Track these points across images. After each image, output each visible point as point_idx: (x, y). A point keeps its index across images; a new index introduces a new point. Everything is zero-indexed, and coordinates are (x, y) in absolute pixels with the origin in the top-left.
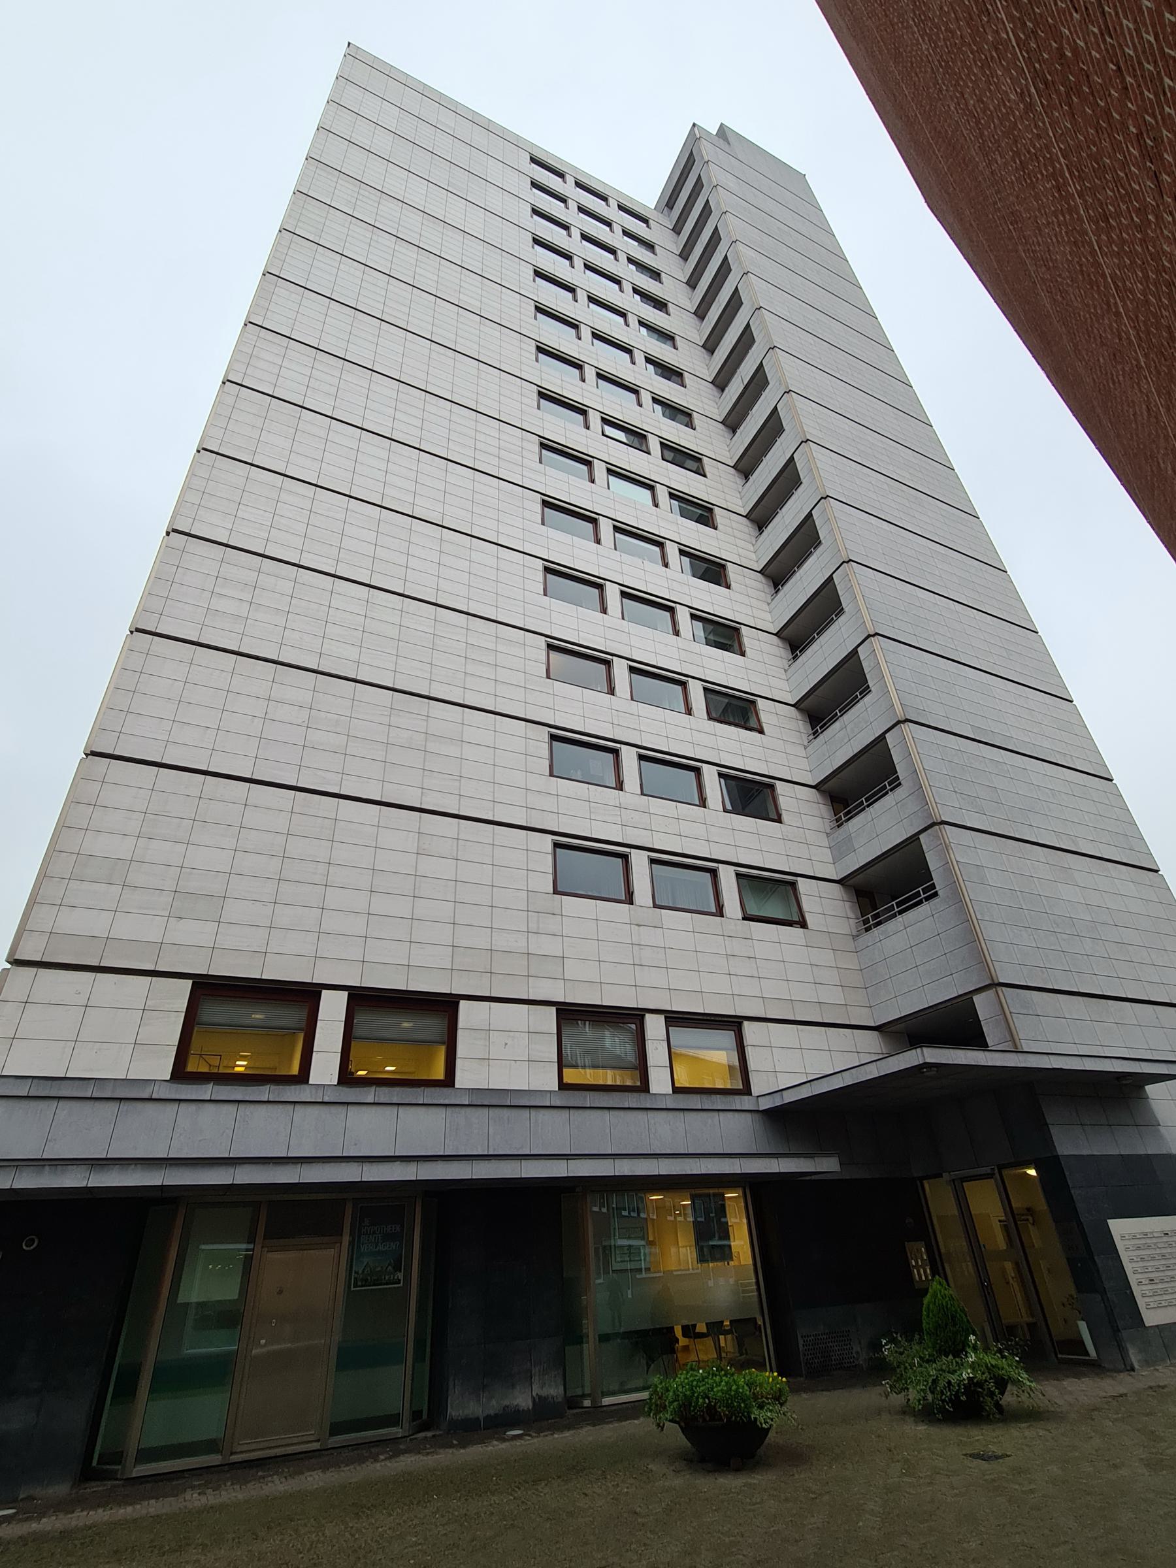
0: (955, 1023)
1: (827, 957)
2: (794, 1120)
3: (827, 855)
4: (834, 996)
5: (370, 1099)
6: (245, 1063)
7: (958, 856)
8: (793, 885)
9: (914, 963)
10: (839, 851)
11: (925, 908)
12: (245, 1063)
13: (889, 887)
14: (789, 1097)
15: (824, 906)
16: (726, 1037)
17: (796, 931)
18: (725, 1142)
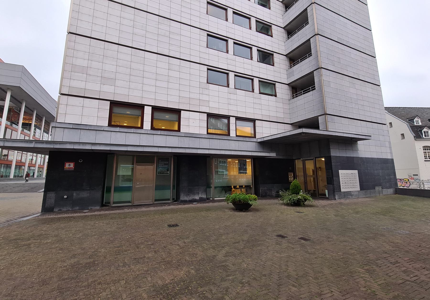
0: (313, 123)
1: (281, 105)
9: (305, 107)
10: (289, 76)
16: (251, 124)
17: (273, 98)
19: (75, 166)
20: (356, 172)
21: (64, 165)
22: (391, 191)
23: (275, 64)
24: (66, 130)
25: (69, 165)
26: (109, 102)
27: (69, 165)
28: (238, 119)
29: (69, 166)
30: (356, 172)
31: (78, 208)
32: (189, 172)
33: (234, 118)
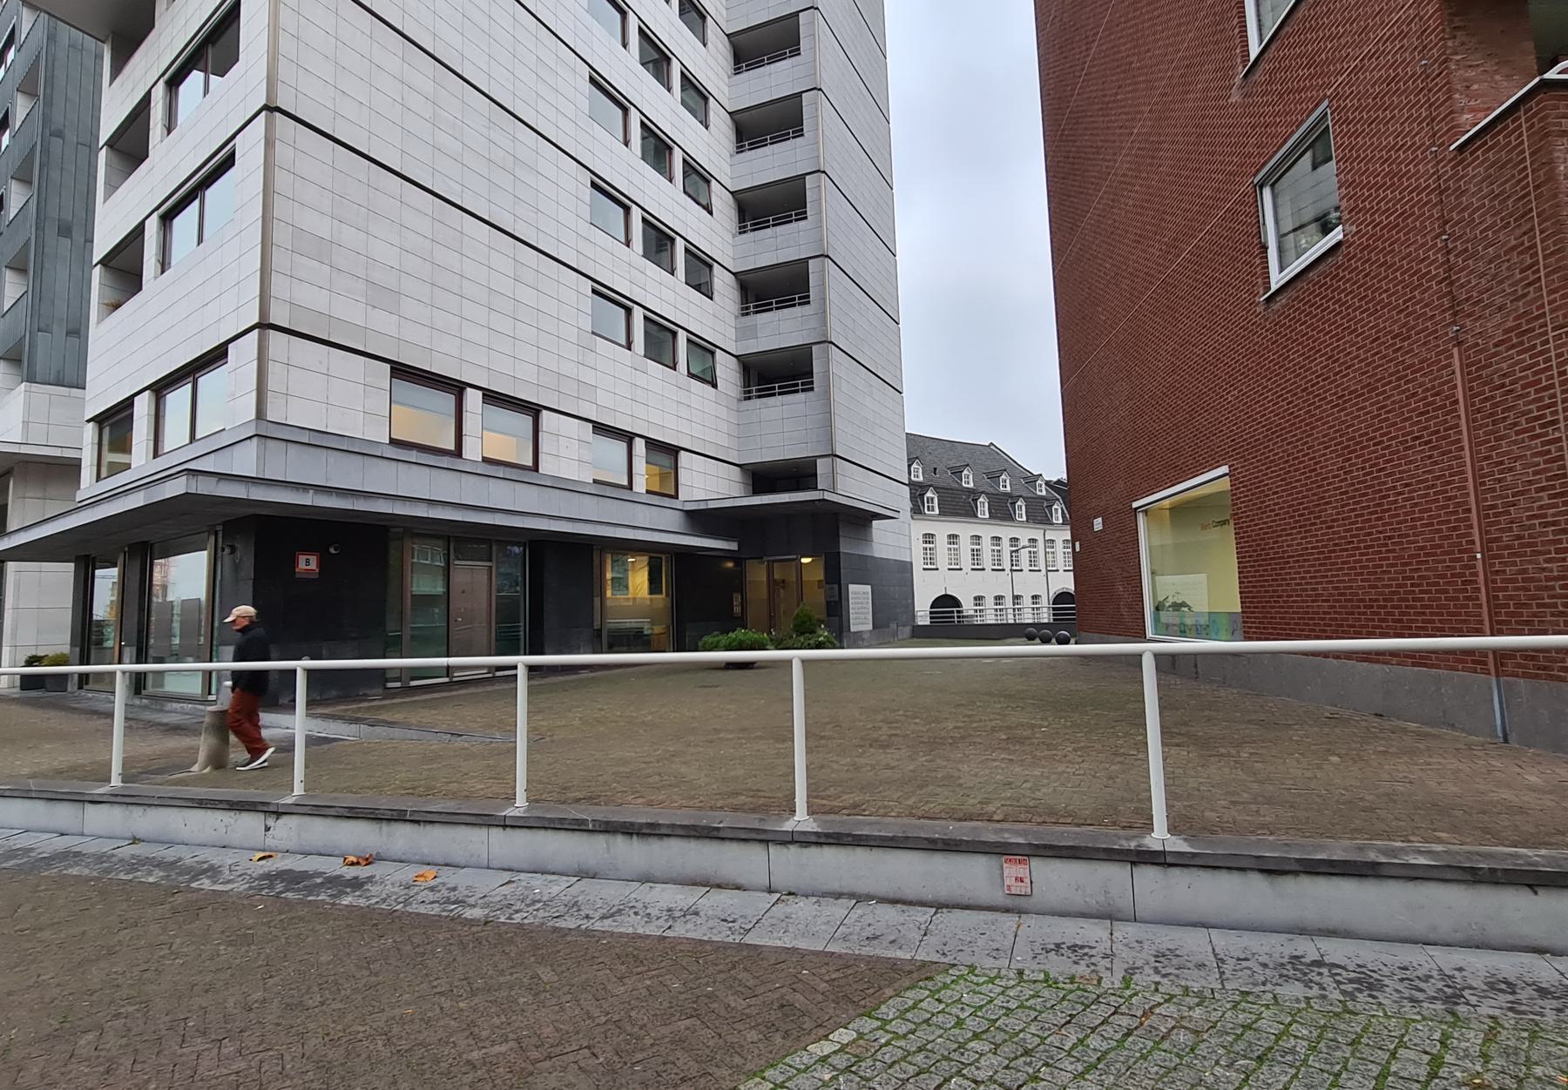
0: (799, 474)
1: (723, 413)
2: (701, 519)
3: (732, 333)
4: (724, 441)
5: (802, 909)
6: (1224, 469)
7: (834, 368)
8: (713, 353)
9: (780, 427)
10: (742, 334)
11: (801, 396)
12: (1224, 469)
13: (777, 374)
14: (712, 505)
15: (727, 370)
16: (524, 422)
17: (708, 388)
18: (661, 525)
19: (320, 564)
20: (868, 588)
21: (294, 563)
22: (908, 629)
23: (716, 296)
24: (293, 448)
25: (308, 562)
26: (388, 366)
27: (308, 562)
28: (492, 397)
29: (307, 564)
30: (868, 588)
31: (334, 693)
32: (549, 582)
33: (388, 366)
